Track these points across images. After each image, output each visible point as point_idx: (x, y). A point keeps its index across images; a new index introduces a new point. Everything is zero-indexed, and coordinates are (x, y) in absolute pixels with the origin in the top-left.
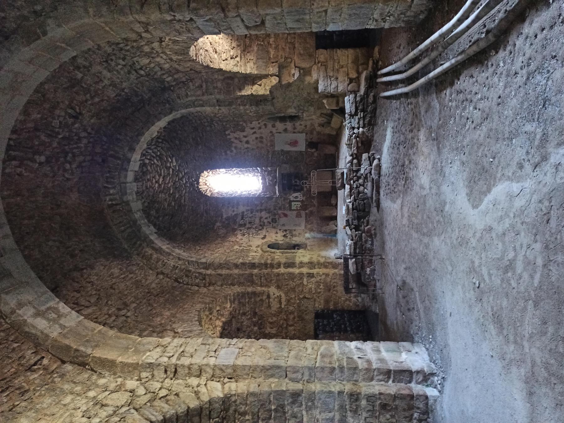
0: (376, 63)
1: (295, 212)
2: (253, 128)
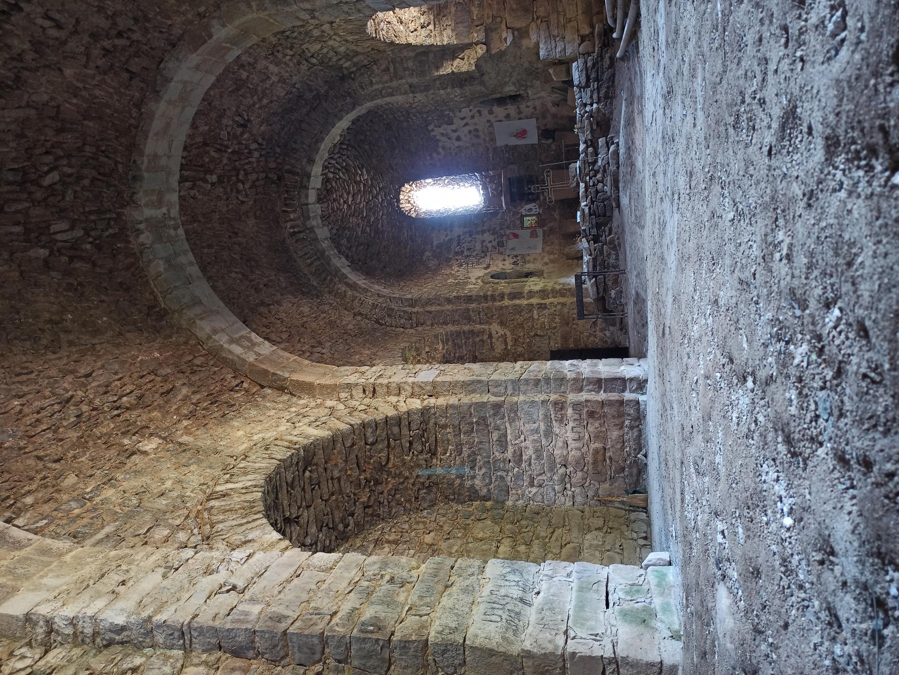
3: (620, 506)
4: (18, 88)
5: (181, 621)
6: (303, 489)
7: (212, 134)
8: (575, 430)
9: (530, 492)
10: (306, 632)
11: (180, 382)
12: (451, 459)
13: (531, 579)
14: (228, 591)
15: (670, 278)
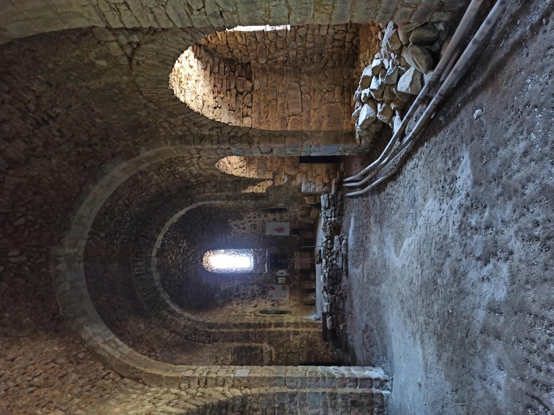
0: (341, 174)
2: (250, 218)
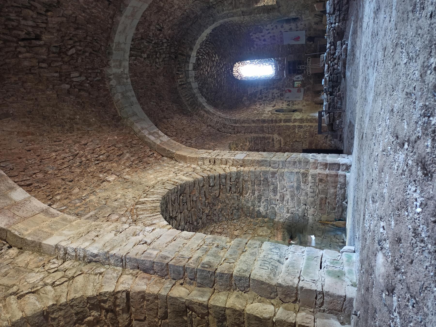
1: (297, 89)
3: (331, 226)
4: (59, 7)
5: (122, 254)
6: (179, 204)
7: (145, 33)
8: (312, 187)
9: (287, 216)
10: (177, 265)
11: (126, 151)
12: (250, 197)
13: (284, 252)
14: (143, 244)
15: (368, 109)
